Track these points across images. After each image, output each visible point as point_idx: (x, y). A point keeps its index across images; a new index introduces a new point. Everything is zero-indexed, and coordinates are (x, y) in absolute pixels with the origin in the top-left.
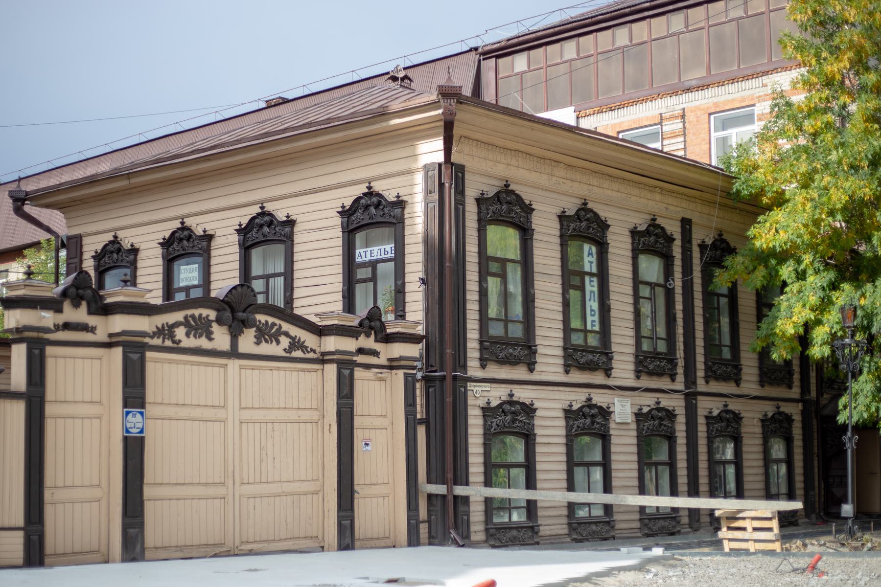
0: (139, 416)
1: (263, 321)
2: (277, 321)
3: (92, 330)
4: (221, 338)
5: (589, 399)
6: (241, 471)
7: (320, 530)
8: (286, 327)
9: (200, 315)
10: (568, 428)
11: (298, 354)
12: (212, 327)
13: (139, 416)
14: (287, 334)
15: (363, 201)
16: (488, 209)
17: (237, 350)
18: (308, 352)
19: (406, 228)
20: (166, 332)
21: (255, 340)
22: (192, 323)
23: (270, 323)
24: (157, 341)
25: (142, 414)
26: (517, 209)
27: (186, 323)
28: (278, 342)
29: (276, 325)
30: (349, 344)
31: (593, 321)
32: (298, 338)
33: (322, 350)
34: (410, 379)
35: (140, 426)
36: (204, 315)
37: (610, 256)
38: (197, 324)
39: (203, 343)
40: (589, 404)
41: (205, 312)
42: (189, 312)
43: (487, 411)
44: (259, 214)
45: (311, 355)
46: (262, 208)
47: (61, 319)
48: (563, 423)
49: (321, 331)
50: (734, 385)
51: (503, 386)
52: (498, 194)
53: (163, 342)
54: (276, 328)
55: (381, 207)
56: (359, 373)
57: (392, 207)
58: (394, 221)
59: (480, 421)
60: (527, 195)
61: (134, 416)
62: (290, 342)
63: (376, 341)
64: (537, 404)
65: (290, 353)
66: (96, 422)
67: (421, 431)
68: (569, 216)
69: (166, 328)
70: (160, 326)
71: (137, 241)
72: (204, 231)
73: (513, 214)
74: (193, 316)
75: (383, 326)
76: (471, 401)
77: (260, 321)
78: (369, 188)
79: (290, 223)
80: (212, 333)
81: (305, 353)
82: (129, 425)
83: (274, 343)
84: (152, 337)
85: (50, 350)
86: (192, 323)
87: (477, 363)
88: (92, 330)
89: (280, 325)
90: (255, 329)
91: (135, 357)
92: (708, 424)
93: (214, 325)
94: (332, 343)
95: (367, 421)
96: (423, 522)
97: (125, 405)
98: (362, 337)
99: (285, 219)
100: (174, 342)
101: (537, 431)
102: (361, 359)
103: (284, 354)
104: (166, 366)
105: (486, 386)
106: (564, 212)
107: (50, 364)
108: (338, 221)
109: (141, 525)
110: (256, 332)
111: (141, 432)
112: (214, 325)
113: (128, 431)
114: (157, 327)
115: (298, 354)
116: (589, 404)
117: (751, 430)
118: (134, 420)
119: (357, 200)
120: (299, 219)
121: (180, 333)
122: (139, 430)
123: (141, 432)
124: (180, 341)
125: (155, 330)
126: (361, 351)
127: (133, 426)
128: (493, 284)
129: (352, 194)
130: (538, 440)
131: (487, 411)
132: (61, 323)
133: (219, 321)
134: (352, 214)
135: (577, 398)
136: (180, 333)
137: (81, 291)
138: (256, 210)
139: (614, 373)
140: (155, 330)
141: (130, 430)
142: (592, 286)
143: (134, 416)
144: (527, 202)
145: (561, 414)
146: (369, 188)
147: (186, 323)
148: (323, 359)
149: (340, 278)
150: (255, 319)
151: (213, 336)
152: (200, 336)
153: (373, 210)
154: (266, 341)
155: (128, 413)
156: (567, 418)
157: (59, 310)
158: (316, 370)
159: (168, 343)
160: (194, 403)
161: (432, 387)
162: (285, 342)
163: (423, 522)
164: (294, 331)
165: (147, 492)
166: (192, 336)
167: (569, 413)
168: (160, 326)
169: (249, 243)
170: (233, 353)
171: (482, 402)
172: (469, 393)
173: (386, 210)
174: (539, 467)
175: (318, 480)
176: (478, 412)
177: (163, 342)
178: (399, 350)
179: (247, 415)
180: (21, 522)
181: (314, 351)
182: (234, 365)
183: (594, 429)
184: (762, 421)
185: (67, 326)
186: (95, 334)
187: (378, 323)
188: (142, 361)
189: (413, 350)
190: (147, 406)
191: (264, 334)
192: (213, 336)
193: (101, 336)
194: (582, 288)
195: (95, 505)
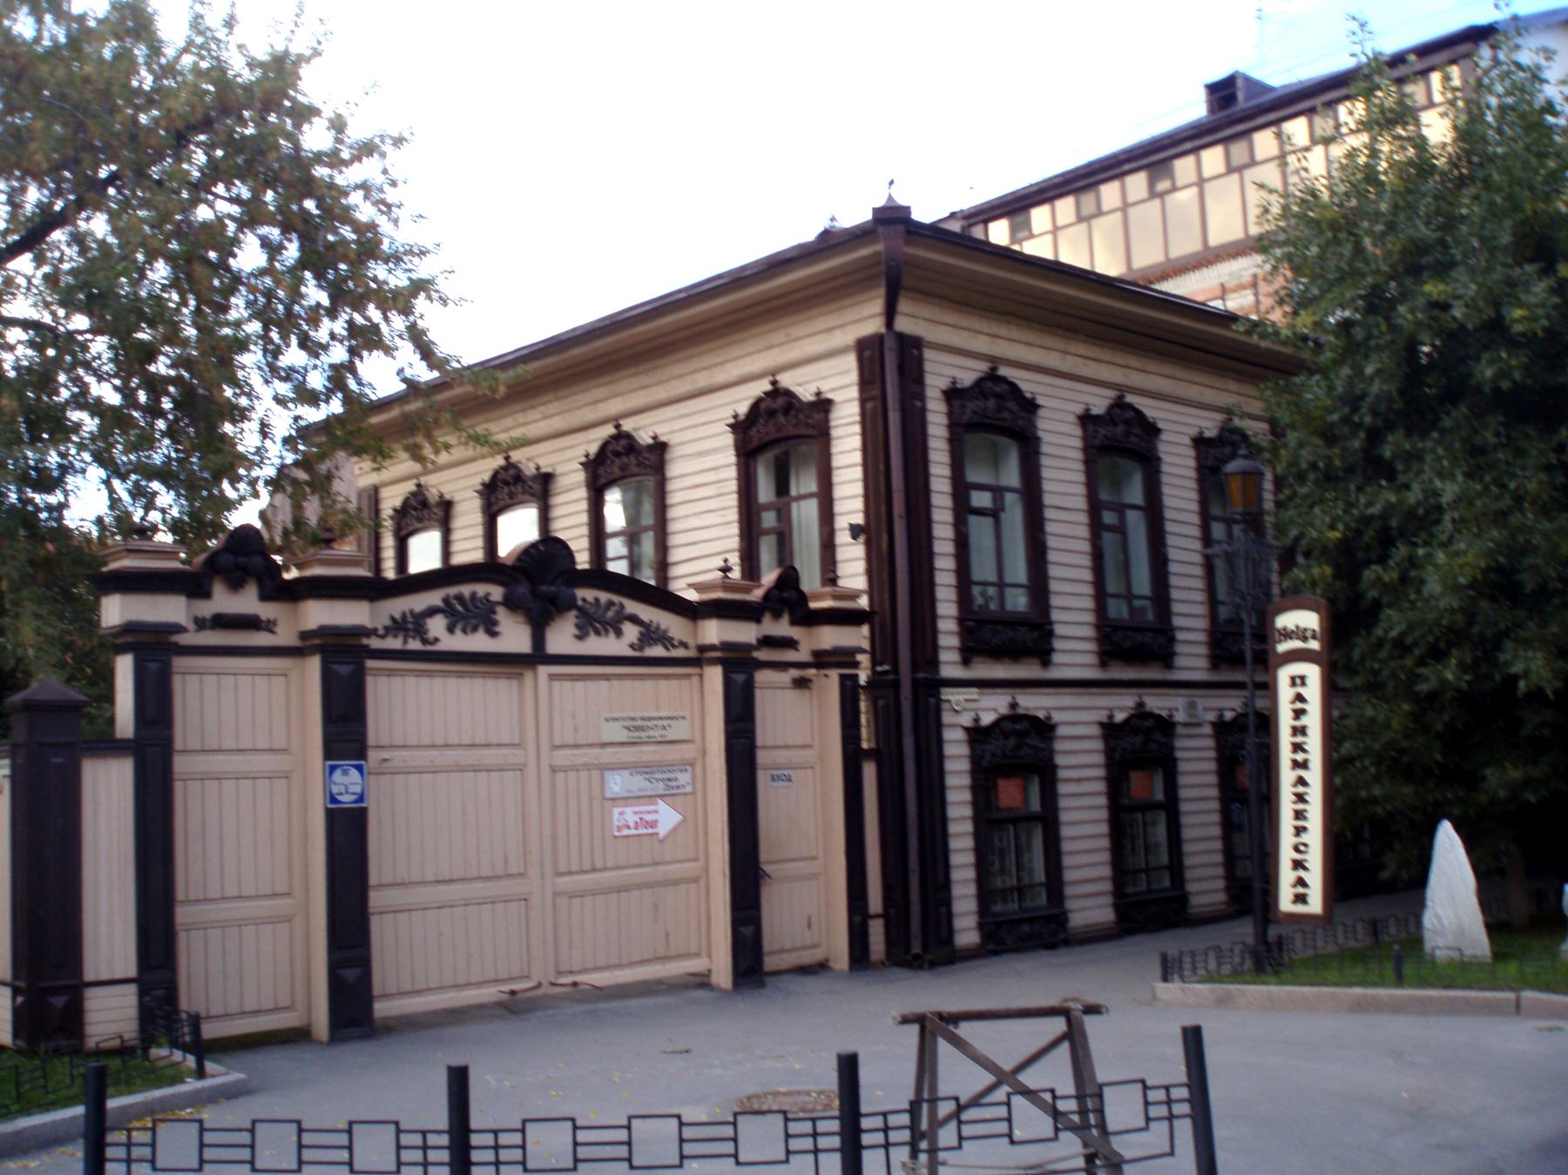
2: (616, 598)
4: (514, 636)
5: (1141, 705)
6: (555, 851)
7: (704, 943)
8: (632, 607)
9: (473, 595)
10: (1109, 752)
11: (657, 651)
13: (354, 773)
14: (634, 620)
15: (763, 405)
16: (964, 407)
18: (674, 646)
20: (410, 626)
21: (576, 632)
22: (459, 608)
25: (359, 768)
26: (1012, 405)
27: (447, 609)
28: (619, 633)
30: (744, 633)
31: (1142, 581)
32: (408, 615)
34: (849, 683)
35: (358, 789)
37: (1165, 479)
39: (478, 642)
40: (1141, 713)
41: (481, 589)
42: (453, 591)
43: (977, 734)
45: (680, 653)
46: (618, 427)
47: (207, 609)
48: (1098, 745)
49: (693, 612)
51: (1183, 692)
52: (979, 383)
53: (405, 642)
55: (793, 413)
56: (762, 676)
59: (964, 750)
61: (345, 773)
62: (641, 633)
63: (264, 597)
64: (1057, 717)
66: (280, 784)
67: (869, 772)
68: (1097, 417)
69: (410, 619)
70: (398, 616)
71: (449, 491)
72: (538, 468)
74: (459, 598)
75: (803, 598)
76: (947, 718)
77: (584, 600)
78: (774, 383)
80: (495, 623)
81: (668, 649)
82: (335, 789)
84: (383, 637)
85: (179, 663)
86: (459, 608)
87: (955, 656)
94: (713, 631)
95: (781, 756)
96: (876, 916)
97: (329, 753)
98: (767, 619)
99: (650, 441)
100: (425, 641)
101: (1060, 760)
102: (762, 655)
103: (630, 653)
105: (972, 693)
106: (1088, 410)
108: (729, 439)
109: (365, 963)
111: (361, 798)
115: (657, 651)
116: (1141, 713)
118: (345, 780)
119: (755, 406)
121: (437, 626)
122: (353, 797)
123: (361, 798)
124: (437, 640)
125: (388, 622)
126: (767, 642)
127: (343, 789)
128: (980, 530)
131: (977, 734)
133: (510, 603)
135: (1121, 705)
136: (437, 626)
137: (242, 560)
138: (609, 430)
139: (1180, 661)
140: (388, 622)
141: (338, 797)
142: (1136, 523)
143: (345, 773)
144: (1028, 395)
145: (1095, 731)
146: (774, 383)
147: (447, 609)
148: (699, 659)
149: (735, 529)
150: (574, 598)
151: (497, 629)
152: (475, 629)
154: (598, 633)
155: (333, 769)
157: (758, 621)
158: (689, 676)
159: (415, 645)
160: (464, 742)
162: (631, 632)
163: (876, 916)
164: (647, 613)
167: (1110, 730)
168: (398, 616)
170: (539, 656)
171: (966, 720)
172: (945, 706)
173: (801, 417)
174: (1064, 817)
175: (695, 860)
176: (960, 735)
177: (405, 642)
178: (830, 637)
179: (563, 758)
180: (131, 970)
181: (685, 645)
182: (544, 671)
184: (1214, 724)
187: (794, 594)
189: (858, 637)
191: (591, 622)
192: (497, 629)
193: (284, 636)
194: (1121, 530)
195: (283, 928)
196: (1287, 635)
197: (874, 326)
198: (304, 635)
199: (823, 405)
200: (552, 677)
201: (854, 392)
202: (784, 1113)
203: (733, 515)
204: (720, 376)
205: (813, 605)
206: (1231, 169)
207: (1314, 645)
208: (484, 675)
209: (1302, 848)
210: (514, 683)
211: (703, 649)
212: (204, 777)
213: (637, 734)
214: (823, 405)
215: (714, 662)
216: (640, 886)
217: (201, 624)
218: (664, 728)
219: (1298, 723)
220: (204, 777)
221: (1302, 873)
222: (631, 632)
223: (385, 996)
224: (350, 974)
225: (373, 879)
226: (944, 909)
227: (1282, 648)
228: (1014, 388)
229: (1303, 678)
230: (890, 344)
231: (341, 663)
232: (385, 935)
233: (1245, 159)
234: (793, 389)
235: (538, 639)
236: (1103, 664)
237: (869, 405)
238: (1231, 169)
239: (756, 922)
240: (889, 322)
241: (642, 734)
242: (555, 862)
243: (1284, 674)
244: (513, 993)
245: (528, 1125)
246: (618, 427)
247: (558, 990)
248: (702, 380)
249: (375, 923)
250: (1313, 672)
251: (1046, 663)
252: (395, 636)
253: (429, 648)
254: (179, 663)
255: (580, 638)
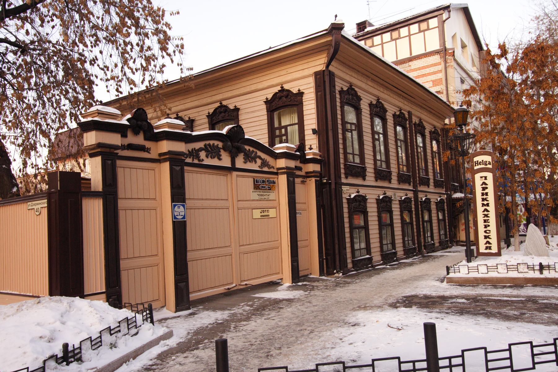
0: (181, 207)
1: (247, 149)
2: (255, 150)
3: (148, 150)
4: (226, 161)
8: (259, 153)
9: (214, 144)
12: (220, 152)
13: (182, 207)
14: (260, 158)
17: (235, 166)
19: (304, 107)
21: (243, 160)
23: (251, 150)
24: (189, 160)
25: (183, 206)
27: (205, 149)
28: (256, 162)
29: (254, 152)
33: (277, 167)
36: (216, 144)
38: (212, 150)
39: (215, 162)
41: (216, 143)
44: (219, 107)
45: (272, 170)
46: (221, 103)
48: (376, 206)
50: (427, 187)
53: (193, 160)
54: (254, 153)
55: (289, 97)
57: (296, 97)
58: (297, 103)
60: (360, 93)
65: (262, 168)
70: (190, 150)
72: (189, 118)
73: (354, 101)
74: (209, 145)
77: (246, 149)
78: (282, 87)
79: (237, 110)
80: (221, 155)
82: (176, 214)
83: (254, 162)
88: (148, 150)
89: (256, 152)
90: (243, 154)
91: (178, 168)
92: (348, 203)
93: (222, 151)
97: (173, 201)
100: (199, 160)
104: (195, 175)
107: (120, 173)
108: (264, 107)
110: (244, 155)
111: (184, 218)
112: (222, 151)
113: (175, 218)
114: (189, 151)
115: (266, 169)
117: (433, 207)
120: (241, 107)
121: (203, 154)
122: (182, 217)
123: (184, 218)
124: (203, 160)
127: (178, 214)
129: (271, 92)
130: (369, 214)
132: (126, 144)
133: (224, 149)
134: (272, 102)
138: (218, 104)
141: (177, 217)
143: (179, 207)
145: (375, 201)
146: (282, 87)
151: (221, 157)
152: (214, 157)
153: (284, 99)
154: (250, 162)
155: (175, 206)
156: (377, 203)
159: (196, 161)
161: (324, 188)
162: (259, 162)
164: (263, 156)
165: (190, 255)
166: (209, 157)
168: (190, 150)
169: (214, 122)
170: (233, 168)
173: (292, 98)
174: (370, 228)
177: (193, 160)
179: (241, 204)
182: (235, 173)
183: (360, 208)
185: (131, 147)
186: (150, 153)
188: (182, 172)
190: (187, 201)
191: (249, 158)
192: (221, 157)
194: (378, 140)
196: (478, 163)
197: (322, 68)
198: (160, 155)
199: (300, 94)
200: (237, 176)
201: (313, 90)
202: (531, 343)
203: (266, 131)
204: (260, 86)
205: (307, 157)
206: (392, 40)
207: (490, 166)
208: (217, 174)
209: (488, 232)
210: (225, 177)
211: (279, 169)
212: (227, 181)
213: (261, 197)
214: (300, 94)
215: (283, 173)
216: (265, 250)
217: (123, 147)
218: (268, 195)
219: (484, 192)
220: (227, 181)
221: (488, 240)
222: (259, 162)
223: (194, 292)
224: (182, 285)
225: (189, 248)
226: (345, 256)
227: (476, 168)
228: (356, 92)
229: (486, 178)
230: (326, 73)
231: (176, 166)
232: (193, 269)
233: (397, 36)
234: (290, 89)
235: (233, 162)
236: (376, 181)
237: (319, 94)
238: (392, 40)
239: (297, 261)
240: (327, 66)
241: (263, 197)
242: (239, 243)
243: (477, 176)
244: (228, 289)
245: (531, 366)
246: (221, 103)
247: (242, 287)
248: (253, 87)
249: (189, 264)
250: (490, 176)
251: (364, 179)
252: (190, 158)
253: (201, 163)
254: (119, 163)
255: (245, 163)
